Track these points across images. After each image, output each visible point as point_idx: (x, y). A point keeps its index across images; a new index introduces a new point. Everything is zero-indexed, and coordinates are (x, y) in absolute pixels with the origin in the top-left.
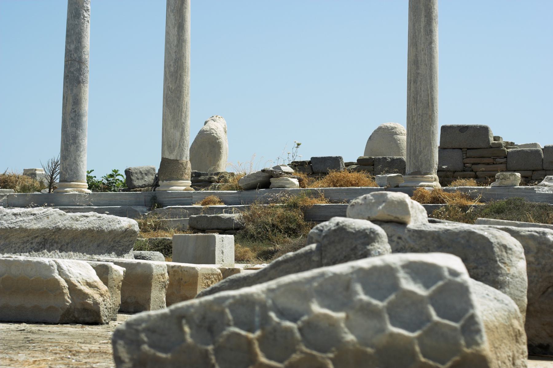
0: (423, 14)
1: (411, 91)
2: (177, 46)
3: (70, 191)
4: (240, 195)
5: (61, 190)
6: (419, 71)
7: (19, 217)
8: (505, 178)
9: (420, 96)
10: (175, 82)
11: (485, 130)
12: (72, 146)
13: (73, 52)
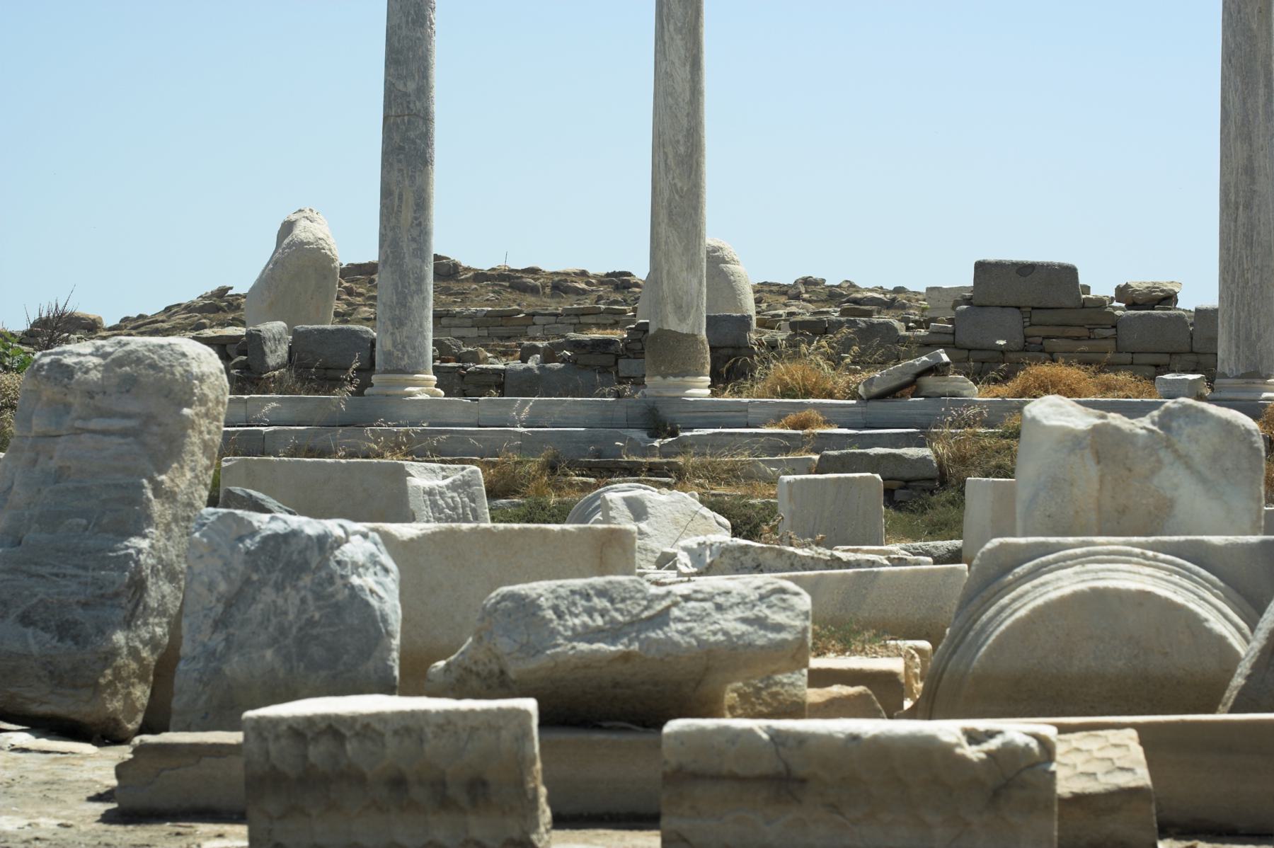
0: (1262, 79)
1: (1239, 223)
4: (865, 410)
5: (399, 391)
6: (1255, 188)
9: (1259, 234)
10: (689, 177)
12: (416, 298)
13: (413, 98)
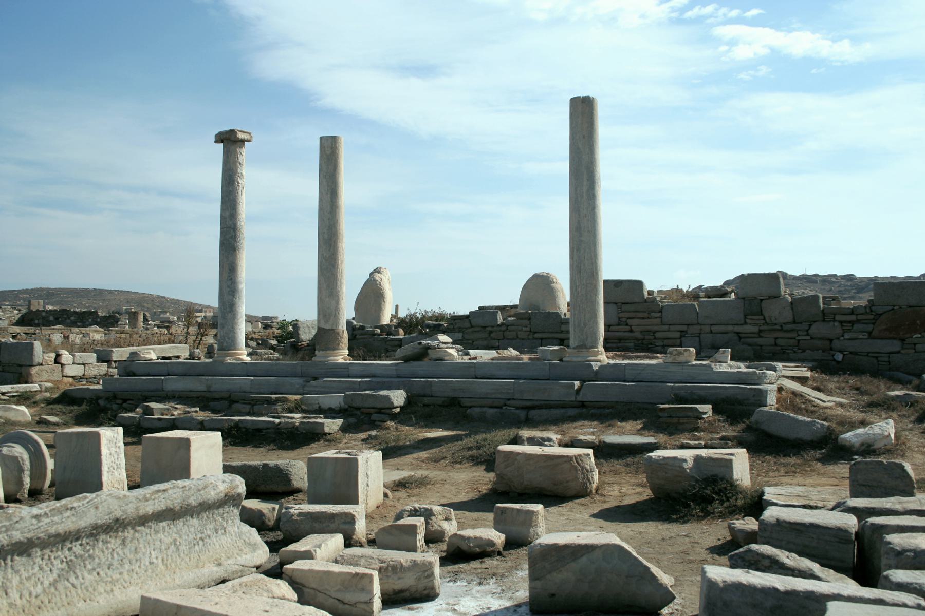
2: (331, 213)
3: (229, 360)
7: (43, 519)
8: (680, 354)
11: (639, 284)
